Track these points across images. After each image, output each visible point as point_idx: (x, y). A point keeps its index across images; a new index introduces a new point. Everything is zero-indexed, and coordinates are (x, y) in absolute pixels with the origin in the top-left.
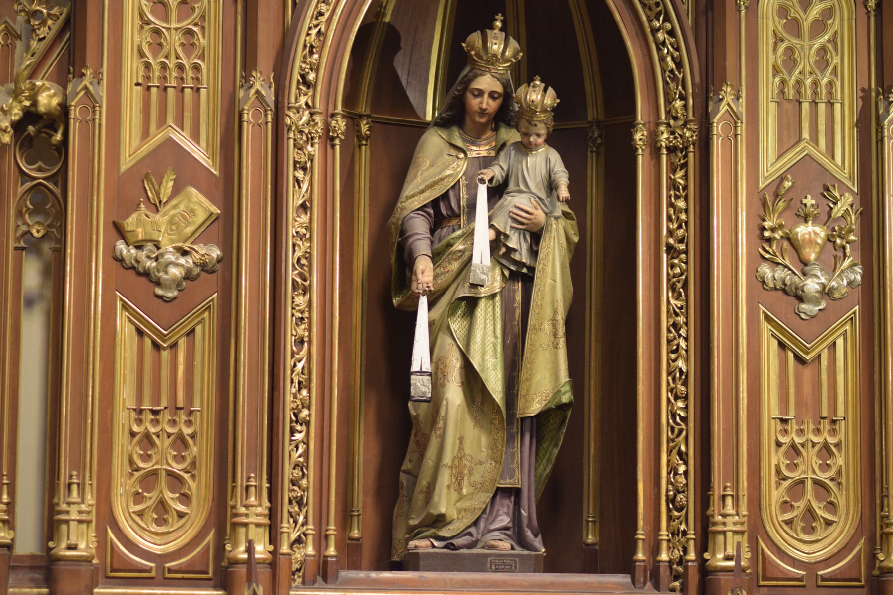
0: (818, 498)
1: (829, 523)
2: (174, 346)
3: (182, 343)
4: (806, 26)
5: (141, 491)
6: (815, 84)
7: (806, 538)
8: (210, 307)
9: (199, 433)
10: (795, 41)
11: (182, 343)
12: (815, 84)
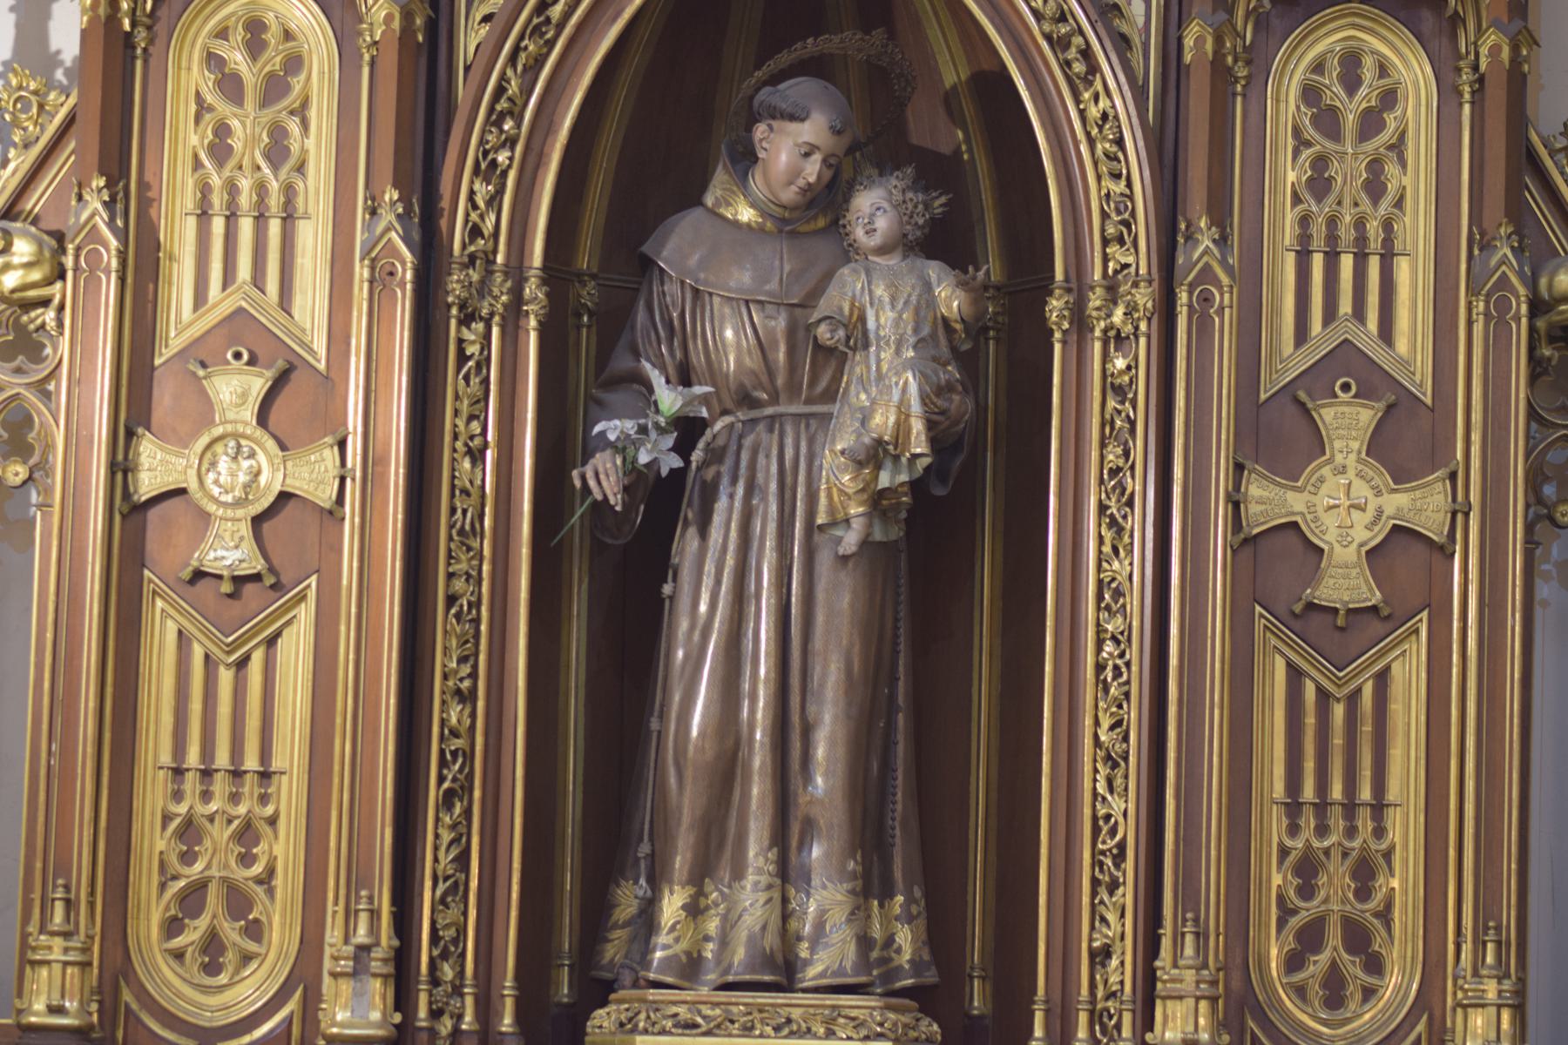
0: (1351, 950)
1: (246, 958)
2: (243, 663)
3: (257, 657)
4: (1350, 120)
5: (180, 916)
6: (1360, 224)
7: (209, 981)
8: (154, 591)
9: (1398, 848)
10: (1330, 145)
11: (257, 657)
12: (1360, 224)
